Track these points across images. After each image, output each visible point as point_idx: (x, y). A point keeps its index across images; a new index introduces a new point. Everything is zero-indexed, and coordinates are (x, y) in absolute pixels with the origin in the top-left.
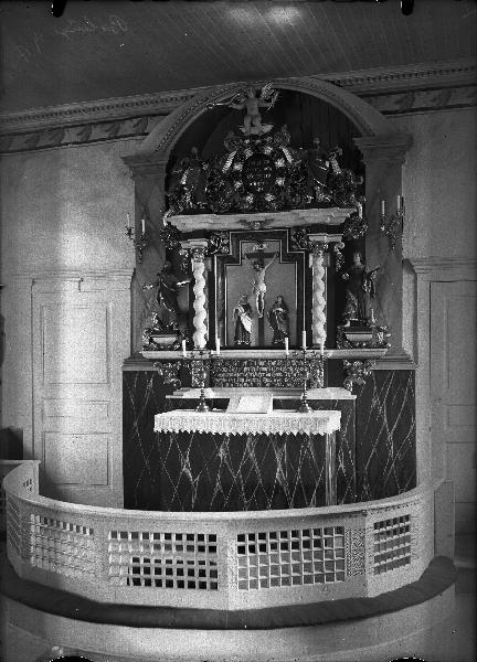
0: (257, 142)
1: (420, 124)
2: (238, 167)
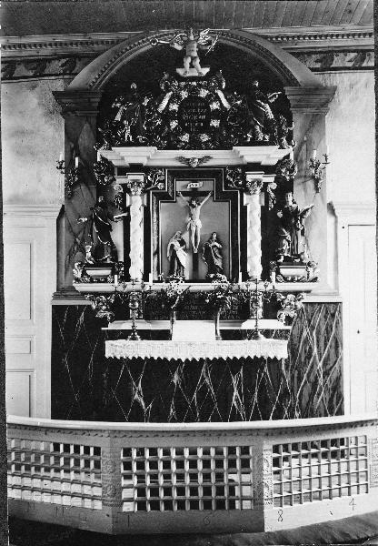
0: (193, 84)
1: (340, 80)
2: (175, 107)
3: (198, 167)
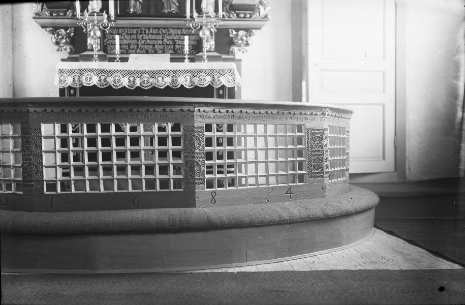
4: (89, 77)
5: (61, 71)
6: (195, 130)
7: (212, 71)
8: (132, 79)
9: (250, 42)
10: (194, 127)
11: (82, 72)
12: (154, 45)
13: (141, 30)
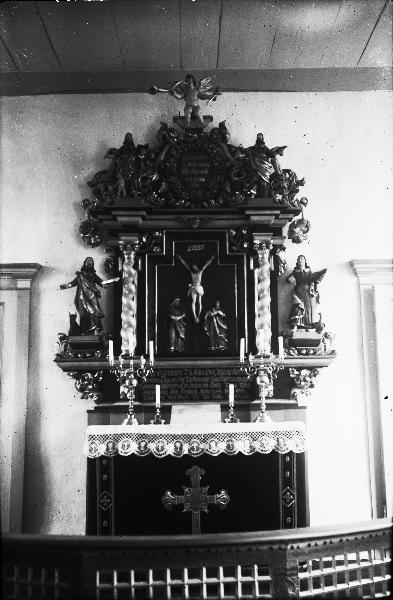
3: (198, 228)
4: (126, 444)
5: (92, 438)
6: (288, 573)
7: (276, 433)
8: (178, 445)
9: (314, 383)
10: (287, 570)
11: (117, 438)
12: (199, 389)
13: (185, 372)
